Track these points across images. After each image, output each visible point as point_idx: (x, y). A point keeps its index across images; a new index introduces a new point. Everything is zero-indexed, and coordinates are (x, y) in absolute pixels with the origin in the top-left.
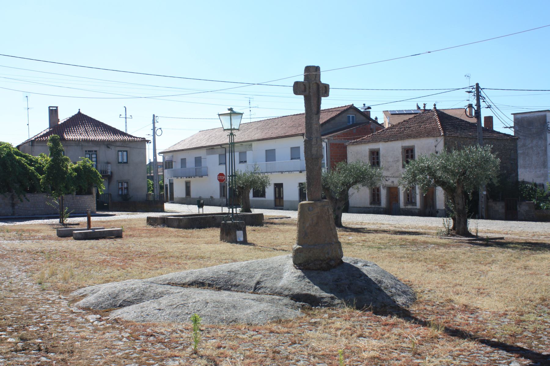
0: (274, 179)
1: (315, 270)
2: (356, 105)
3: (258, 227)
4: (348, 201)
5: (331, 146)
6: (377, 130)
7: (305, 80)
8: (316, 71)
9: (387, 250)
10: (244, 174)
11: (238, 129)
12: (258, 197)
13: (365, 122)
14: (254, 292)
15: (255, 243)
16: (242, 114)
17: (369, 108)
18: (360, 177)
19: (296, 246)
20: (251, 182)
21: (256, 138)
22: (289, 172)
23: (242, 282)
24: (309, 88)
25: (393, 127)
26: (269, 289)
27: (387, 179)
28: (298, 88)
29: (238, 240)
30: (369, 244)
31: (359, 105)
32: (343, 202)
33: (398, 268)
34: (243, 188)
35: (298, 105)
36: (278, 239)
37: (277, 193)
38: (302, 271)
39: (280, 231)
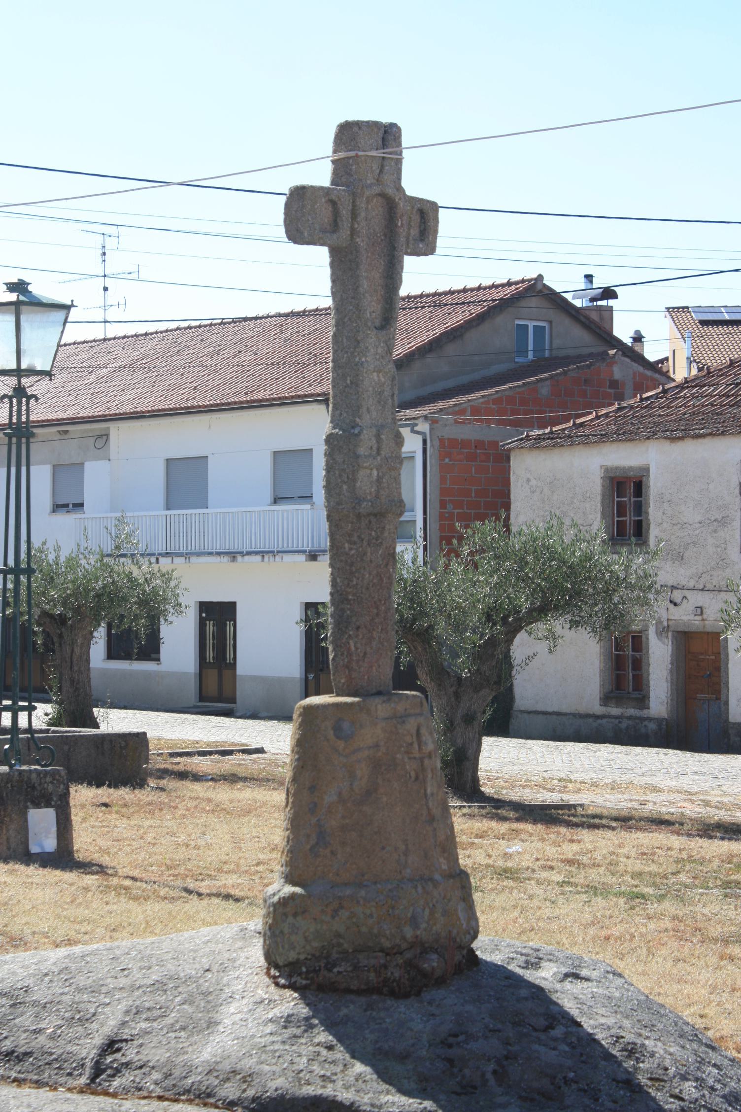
0: (199, 582)
1: (359, 992)
2: (557, 281)
3: (124, 793)
4: (510, 689)
5: (447, 451)
6: (639, 388)
7: (333, 182)
8: (384, 143)
9: (669, 907)
10: (69, 559)
11: (49, 374)
12: (128, 657)
13: (591, 355)
14: (92, 1088)
15: (105, 860)
16: (67, 308)
17: (609, 293)
18: (562, 589)
19: (280, 888)
20: (98, 596)
21: (128, 408)
22: (262, 553)
23: (42, 1039)
24: (354, 215)
25: (707, 376)
26: (156, 1076)
27: (677, 596)
28: (304, 216)
29: (34, 849)
30: (593, 876)
31: (565, 281)
32: (488, 695)
33: (713, 989)
34: (62, 620)
35: (306, 278)
36: (208, 846)
37: (210, 642)
38: (303, 997)
39: (218, 809)
